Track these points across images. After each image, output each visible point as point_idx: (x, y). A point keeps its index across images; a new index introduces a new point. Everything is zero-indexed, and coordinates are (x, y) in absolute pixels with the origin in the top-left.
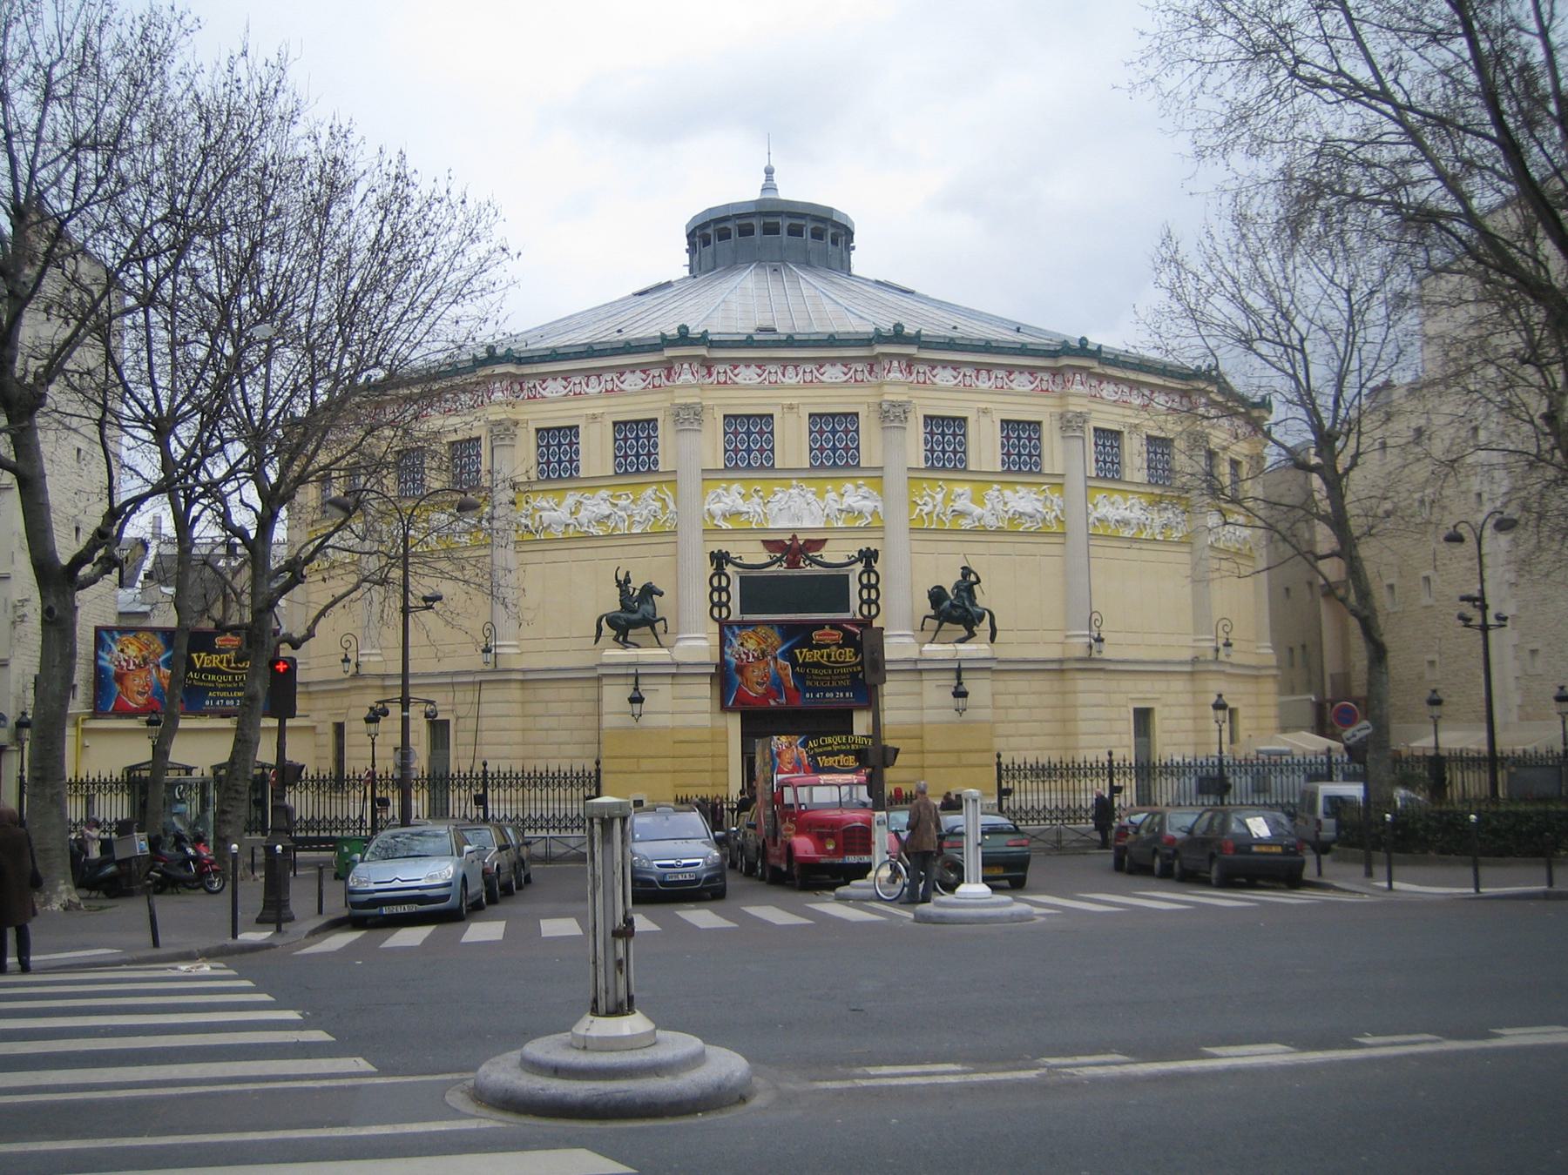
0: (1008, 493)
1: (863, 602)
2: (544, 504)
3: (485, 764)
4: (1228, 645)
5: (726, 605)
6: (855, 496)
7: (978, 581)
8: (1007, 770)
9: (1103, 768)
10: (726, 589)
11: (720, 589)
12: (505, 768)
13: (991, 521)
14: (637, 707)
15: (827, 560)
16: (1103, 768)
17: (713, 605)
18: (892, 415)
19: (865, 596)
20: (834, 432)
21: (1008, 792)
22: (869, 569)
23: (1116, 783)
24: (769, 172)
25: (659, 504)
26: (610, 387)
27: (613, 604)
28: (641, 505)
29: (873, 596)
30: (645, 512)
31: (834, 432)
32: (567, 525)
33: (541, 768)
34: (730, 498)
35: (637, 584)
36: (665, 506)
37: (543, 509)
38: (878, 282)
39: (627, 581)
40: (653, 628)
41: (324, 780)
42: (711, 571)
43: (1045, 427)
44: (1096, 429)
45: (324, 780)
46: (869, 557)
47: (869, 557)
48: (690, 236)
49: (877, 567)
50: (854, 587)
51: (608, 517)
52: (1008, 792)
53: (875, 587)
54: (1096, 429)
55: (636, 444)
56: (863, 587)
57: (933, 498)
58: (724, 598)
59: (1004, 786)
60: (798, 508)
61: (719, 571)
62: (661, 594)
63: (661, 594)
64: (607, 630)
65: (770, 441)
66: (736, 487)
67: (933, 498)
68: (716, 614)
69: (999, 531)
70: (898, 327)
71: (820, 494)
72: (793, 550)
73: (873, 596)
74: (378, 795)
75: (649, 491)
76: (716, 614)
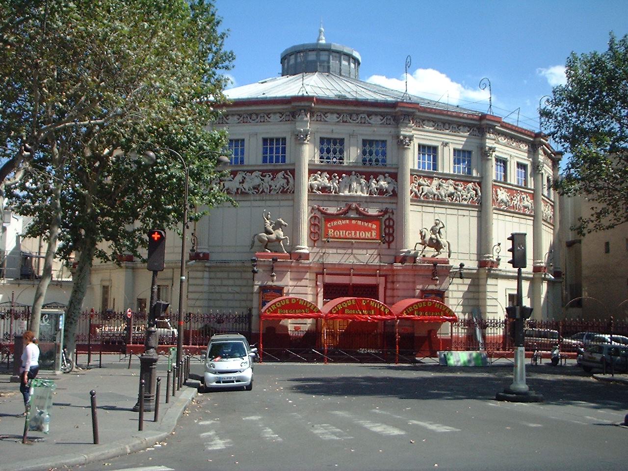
29: (391, 232)
36: (288, 182)
48: (284, 59)
51: (259, 185)
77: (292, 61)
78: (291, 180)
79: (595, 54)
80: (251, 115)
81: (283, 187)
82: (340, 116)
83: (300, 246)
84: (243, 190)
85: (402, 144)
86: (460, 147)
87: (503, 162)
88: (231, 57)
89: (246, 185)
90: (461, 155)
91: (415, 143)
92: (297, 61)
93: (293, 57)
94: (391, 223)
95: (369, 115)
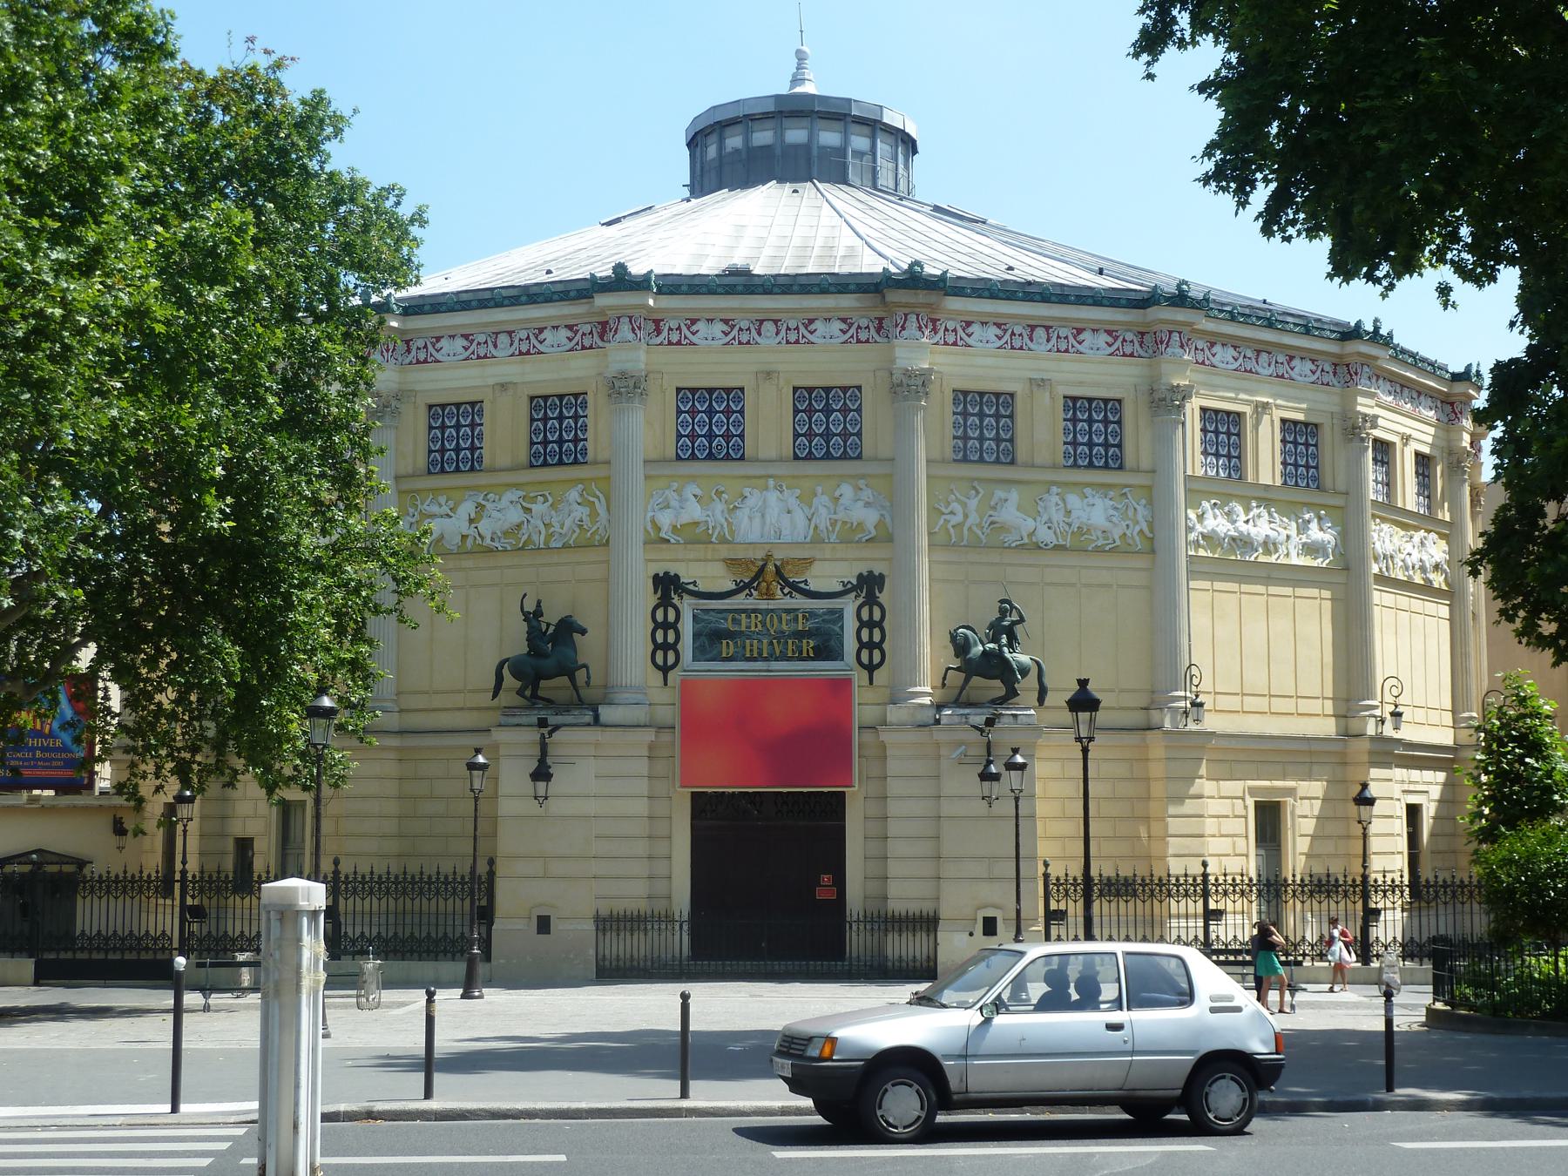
0: (1073, 500)
1: (862, 645)
2: (435, 509)
3: (336, 862)
4: (1396, 715)
5: (674, 647)
6: (849, 500)
7: (1022, 620)
8: (347, 882)
9: (1354, 885)
10: (674, 626)
11: (665, 626)
12: (364, 869)
13: (1045, 535)
14: (541, 785)
15: (814, 586)
16: (1354, 885)
17: (657, 646)
18: (626, 388)
19: (660, 639)
20: (710, 412)
21: (1218, 914)
22: (871, 601)
23: (1212, 906)
24: (801, 57)
25: (586, 511)
26: (524, 349)
27: (516, 643)
28: (564, 507)
29: (877, 638)
30: (568, 522)
31: (710, 412)
32: (464, 537)
33: (429, 870)
34: (689, 501)
35: (551, 617)
36: (594, 514)
37: (433, 516)
38: (937, 209)
39: (538, 613)
40: (573, 679)
41: (149, 881)
42: (653, 600)
43: (590, 399)
44: (1204, 410)
45: (149, 881)
46: (869, 586)
47: (869, 586)
48: (696, 141)
49: (883, 597)
50: (850, 624)
51: (519, 526)
52: (1218, 914)
53: (880, 625)
54: (1204, 410)
55: (558, 431)
56: (862, 624)
57: (964, 505)
58: (671, 638)
59: (1053, 906)
60: (772, 512)
61: (665, 602)
62: (583, 632)
63: (583, 632)
64: (509, 680)
65: (1010, 428)
66: (691, 490)
67: (964, 505)
68: (659, 660)
69: (1058, 548)
70: (620, 269)
71: (806, 499)
72: (763, 574)
73: (877, 638)
74: (189, 901)
75: (573, 495)
76: (659, 660)
77: (712, 151)
78: (601, 509)
79: (315, 108)
80: (1033, 328)
81: (580, 527)
82: (1116, 339)
83: (918, 689)
84: (479, 540)
85: (1165, 403)
86: (1300, 417)
87: (1384, 451)
88: (318, 100)
89: (485, 526)
90: (1297, 434)
91: (1193, 406)
92: (733, 149)
93: (714, 138)
94: (877, 616)
95: (1213, 340)
